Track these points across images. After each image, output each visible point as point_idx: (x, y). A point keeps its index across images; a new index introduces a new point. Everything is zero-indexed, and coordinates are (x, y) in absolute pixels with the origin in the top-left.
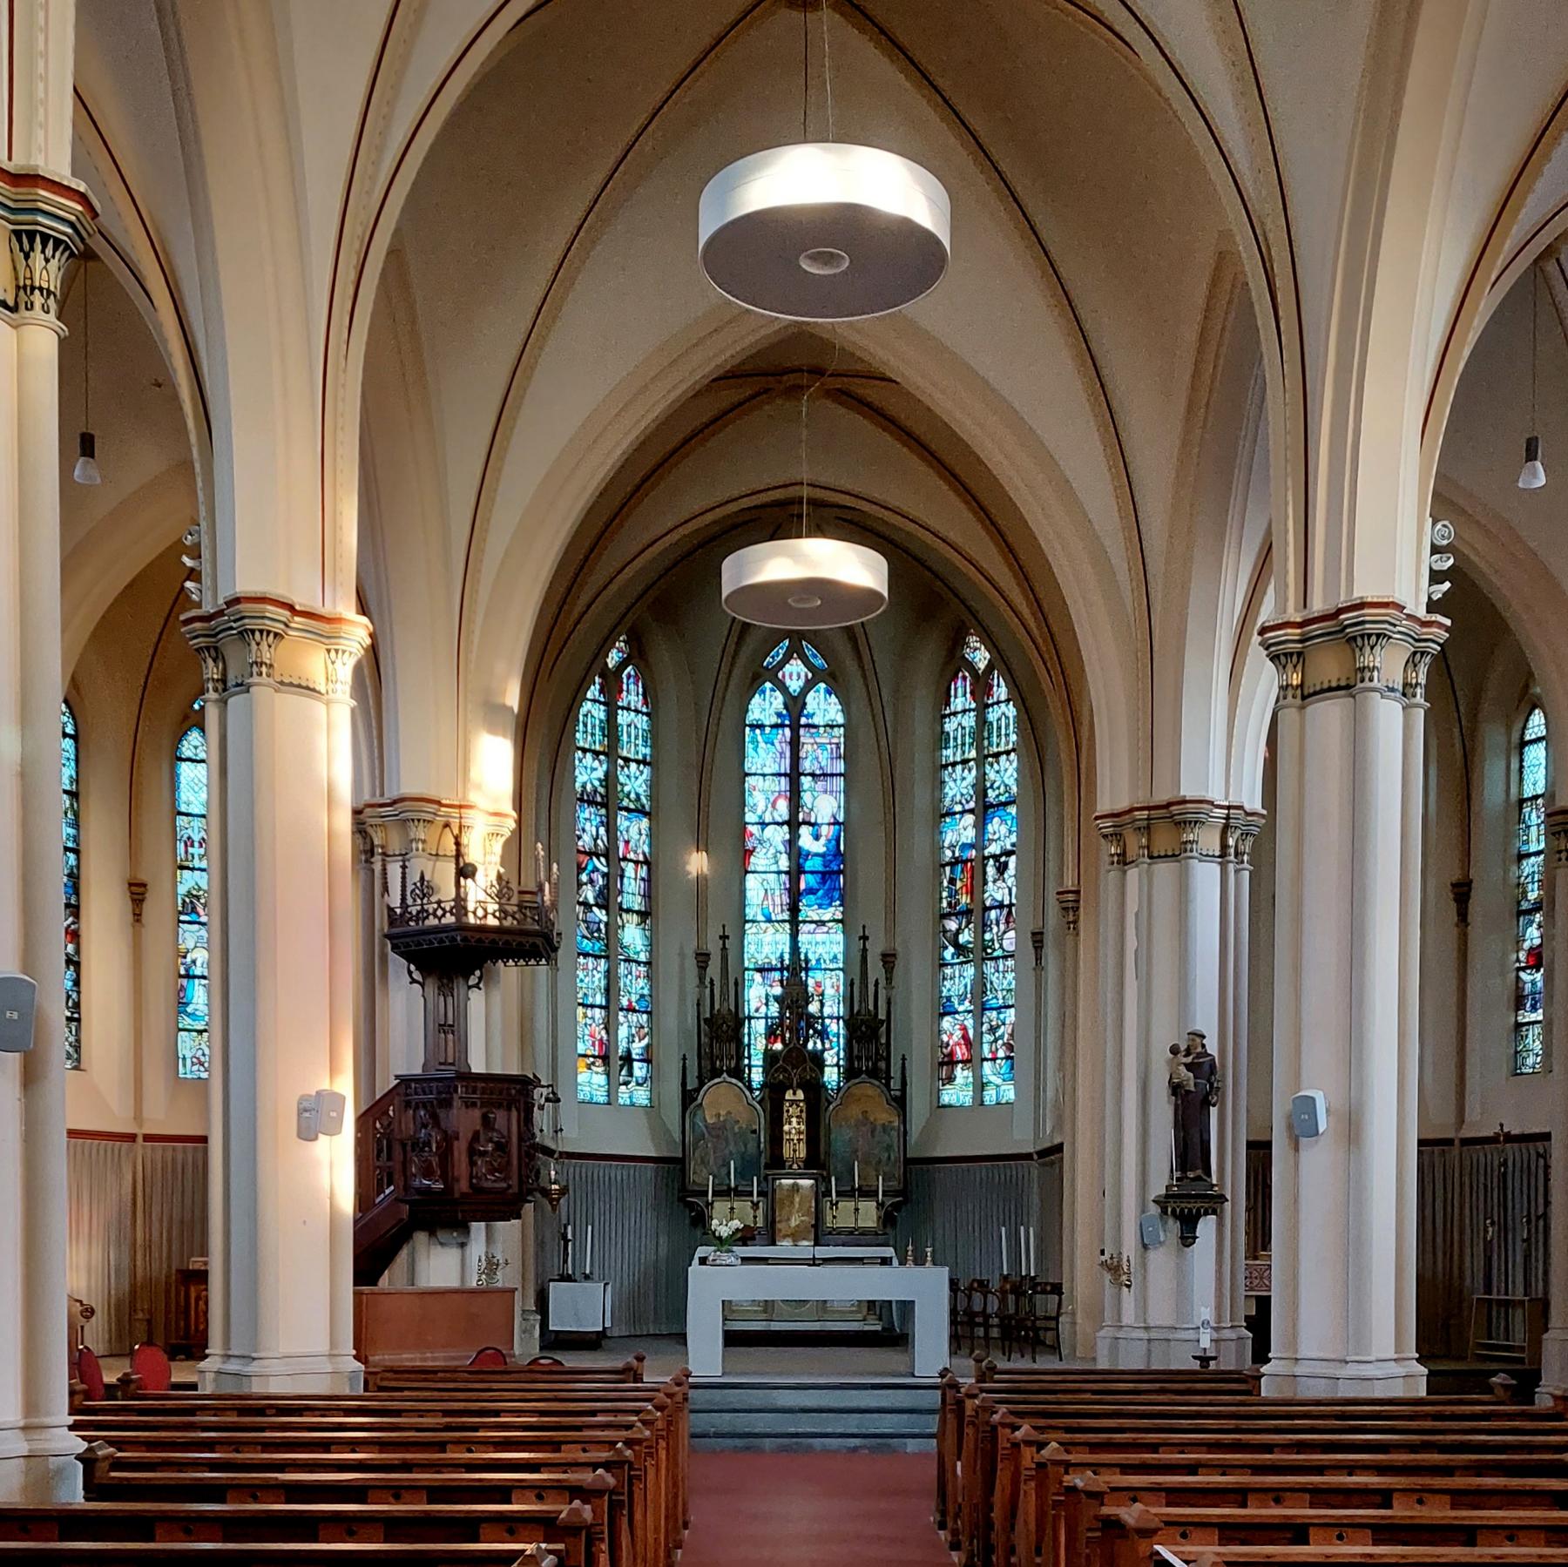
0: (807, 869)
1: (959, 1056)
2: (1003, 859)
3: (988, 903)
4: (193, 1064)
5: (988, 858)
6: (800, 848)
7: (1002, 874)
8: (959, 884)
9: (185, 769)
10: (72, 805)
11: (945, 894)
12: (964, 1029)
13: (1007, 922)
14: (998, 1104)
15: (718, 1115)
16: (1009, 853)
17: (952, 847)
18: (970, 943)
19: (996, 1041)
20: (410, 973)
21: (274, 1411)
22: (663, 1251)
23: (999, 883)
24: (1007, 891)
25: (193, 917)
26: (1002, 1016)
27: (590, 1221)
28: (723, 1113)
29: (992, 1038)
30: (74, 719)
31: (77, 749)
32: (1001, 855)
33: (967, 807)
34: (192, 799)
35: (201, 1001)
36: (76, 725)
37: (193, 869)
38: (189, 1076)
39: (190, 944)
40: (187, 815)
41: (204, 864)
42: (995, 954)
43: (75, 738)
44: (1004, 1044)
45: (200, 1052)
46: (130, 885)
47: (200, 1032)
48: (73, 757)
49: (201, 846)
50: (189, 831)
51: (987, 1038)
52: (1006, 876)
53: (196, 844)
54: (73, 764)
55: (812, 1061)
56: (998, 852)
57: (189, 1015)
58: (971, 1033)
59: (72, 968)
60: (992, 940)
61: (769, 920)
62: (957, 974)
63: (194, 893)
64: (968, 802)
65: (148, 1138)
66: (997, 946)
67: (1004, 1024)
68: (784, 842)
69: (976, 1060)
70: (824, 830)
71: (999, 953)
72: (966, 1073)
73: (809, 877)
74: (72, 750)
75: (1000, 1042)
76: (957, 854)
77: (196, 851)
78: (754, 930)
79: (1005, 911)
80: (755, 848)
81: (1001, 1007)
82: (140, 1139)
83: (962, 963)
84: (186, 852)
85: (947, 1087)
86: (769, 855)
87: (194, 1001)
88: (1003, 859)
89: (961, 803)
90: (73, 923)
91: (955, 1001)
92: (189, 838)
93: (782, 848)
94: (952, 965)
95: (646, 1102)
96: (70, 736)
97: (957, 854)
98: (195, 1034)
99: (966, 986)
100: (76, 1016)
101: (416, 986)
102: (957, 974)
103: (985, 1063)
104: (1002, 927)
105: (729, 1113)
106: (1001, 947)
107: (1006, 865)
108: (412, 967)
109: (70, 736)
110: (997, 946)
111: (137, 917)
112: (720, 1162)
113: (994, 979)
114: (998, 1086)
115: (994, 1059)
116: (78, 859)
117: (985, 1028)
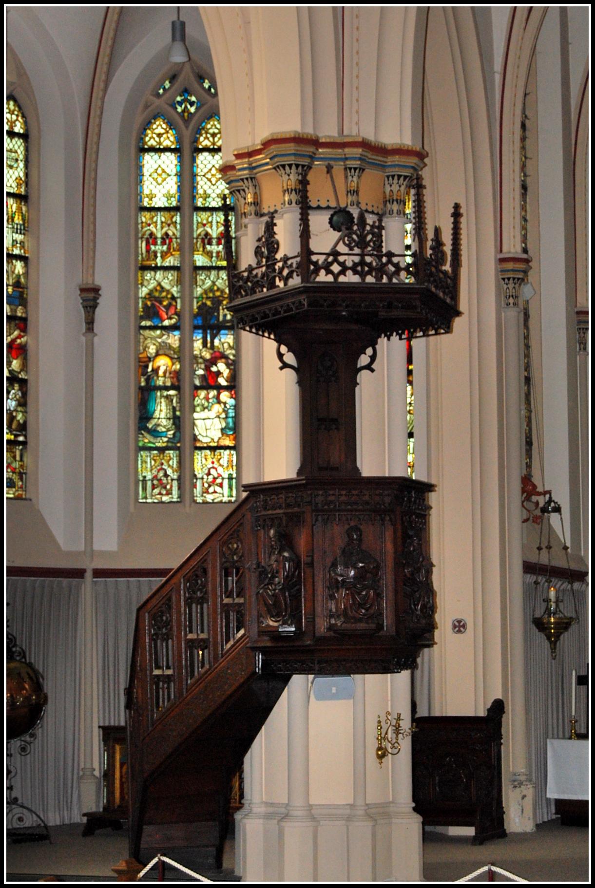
4: (154, 487)
9: (150, 161)
10: (19, 209)
14: (194, 419)
20: (280, 356)
25: (156, 322)
30: (23, 117)
31: (27, 149)
34: (209, 192)
35: (163, 415)
36: (26, 123)
37: (156, 268)
38: (149, 501)
39: (152, 350)
40: (205, 209)
41: (170, 261)
43: (25, 137)
45: (161, 474)
46: (82, 290)
47: (162, 450)
48: (21, 157)
49: (163, 243)
50: (152, 228)
53: (214, 241)
54: (22, 165)
57: (149, 431)
59: (17, 386)
63: (157, 294)
65: (99, 573)
74: (21, 151)
77: (159, 248)
82: (89, 575)
84: (148, 250)
87: (157, 414)
90: (19, 337)
92: (151, 234)
96: (19, 135)
98: (208, 452)
100: (21, 439)
101: (288, 371)
108: (284, 349)
109: (19, 135)
111: (90, 323)
116: (26, 265)
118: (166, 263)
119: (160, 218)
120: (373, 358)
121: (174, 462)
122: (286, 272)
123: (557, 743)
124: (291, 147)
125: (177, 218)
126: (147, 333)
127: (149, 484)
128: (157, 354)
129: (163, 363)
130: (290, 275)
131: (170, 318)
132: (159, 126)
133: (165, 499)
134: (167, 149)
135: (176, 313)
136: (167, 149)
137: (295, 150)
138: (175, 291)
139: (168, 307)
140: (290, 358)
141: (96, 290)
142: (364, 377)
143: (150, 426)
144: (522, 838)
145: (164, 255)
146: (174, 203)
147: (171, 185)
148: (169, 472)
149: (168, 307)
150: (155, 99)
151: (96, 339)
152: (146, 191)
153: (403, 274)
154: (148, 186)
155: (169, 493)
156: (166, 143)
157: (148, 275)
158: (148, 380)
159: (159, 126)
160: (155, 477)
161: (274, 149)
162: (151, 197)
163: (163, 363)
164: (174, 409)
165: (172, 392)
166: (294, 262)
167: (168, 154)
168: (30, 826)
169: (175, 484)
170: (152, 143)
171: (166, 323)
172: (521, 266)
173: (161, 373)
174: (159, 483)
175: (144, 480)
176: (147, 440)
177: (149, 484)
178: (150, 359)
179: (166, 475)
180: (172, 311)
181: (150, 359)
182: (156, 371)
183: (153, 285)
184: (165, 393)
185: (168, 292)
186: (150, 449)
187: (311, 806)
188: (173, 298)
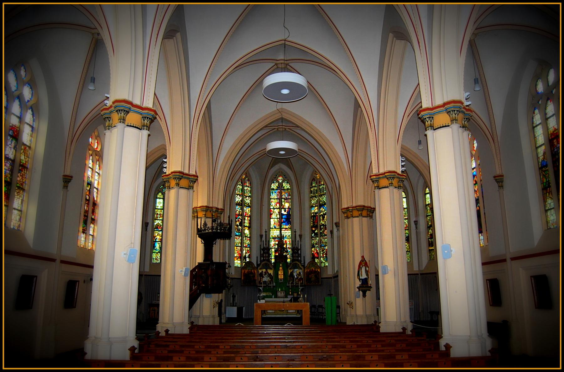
4: (155, 260)
6: (282, 213)
9: (158, 200)
19: (324, 253)
20: (202, 241)
25: (157, 229)
35: (158, 247)
37: (158, 220)
39: (156, 235)
41: (161, 218)
47: (157, 253)
49: (160, 215)
50: (158, 212)
57: (155, 249)
61: (275, 228)
65: (145, 275)
70: (287, 210)
73: (284, 219)
77: (159, 216)
78: (272, 230)
80: (272, 213)
86: (275, 215)
92: (158, 213)
93: (278, 213)
101: (202, 244)
106: (324, 234)
108: (202, 240)
114: (324, 263)
118: (160, 219)
119: (159, 210)
120: (216, 242)
121: (159, 255)
122: (208, 229)
123: (229, 307)
124: (205, 208)
125: (162, 211)
126: (156, 231)
127: (154, 259)
128: (157, 235)
129: (158, 237)
130: (209, 230)
131: (160, 229)
132: (160, 194)
133: (157, 262)
134: (161, 198)
135: (161, 228)
136: (161, 198)
137: (206, 209)
138: (161, 224)
139: (160, 227)
140: (203, 242)
141: (148, 223)
142: (214, 245)
143: (155, 248)
144: (224, 323)
145: (160, 217)
146: (162, 208)
147: (162, 205)
148: (158, 257)
149: (160, 227)
150: (160, 189)
151: (147, 232)
152: (157, 206)
153: (226, 231)
154: (157, 205)
155: (158, 261)
156: (161, 197)
157: (157, 221)
158: (155, 240)
159: (160, 194)
160: (156, 258)
161: (202, 208)
162: (158, 207)
163: (158, 237)
164: (160, 246)
165: (160, 242)
166: (210, 228)
167: (161, 199)
168: (551, 210)
169: (159, 259)
170: (159, 197)
171: (159, 230)
172: (70, 178)
173: (158, 239)
174: (156, 259)
175: (154, 258)
176: (154, 251)
177: (154, 259)
178: (156, 236)
179: (158, 258)
180: (160, 228)
181: (156, 236)
182: (157, 238)
183: (157, 222)
184: (158, 243)
185: (160, 224)
186: (155, 253)
187: (174, 323)
188: (161, 225)
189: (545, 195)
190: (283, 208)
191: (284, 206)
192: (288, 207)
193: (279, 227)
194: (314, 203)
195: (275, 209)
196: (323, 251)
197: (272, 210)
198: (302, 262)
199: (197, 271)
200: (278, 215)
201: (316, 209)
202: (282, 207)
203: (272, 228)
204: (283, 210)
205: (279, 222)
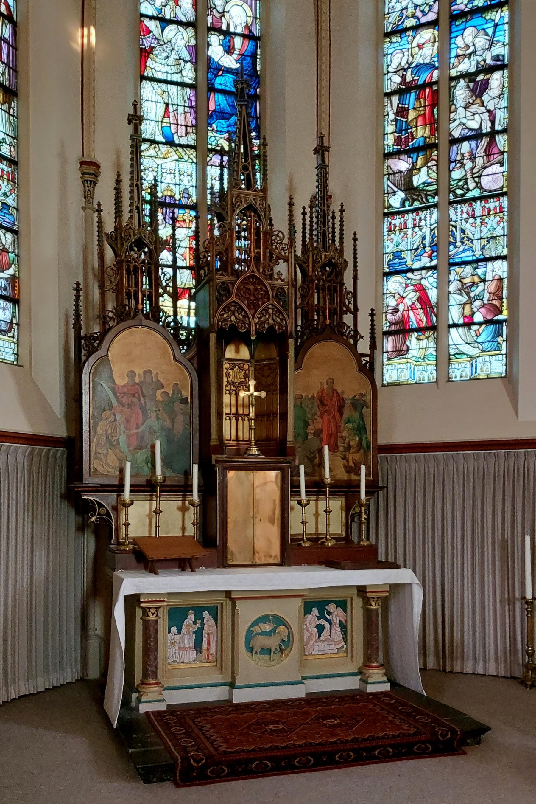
0: (217, 86)
1: (414, 324)
2: (480, 78)
3: (456, 134)
5: (457, 78)
6: (209, 58)
7: (480, 96)
8: (412, 115)
11: (390, 129)
12: (420, 289)
13: (488, 153)
15: (132, 374)
16: (490, 70)
17: (402, 70)
18: (429, 184)
19: (471, 301)
21: (120, 296)
22: (40, 572)
23: (474, 108)
24: (486, 116)
26: (480, 272)
27: (527, 529)
28: (139, 371)
29: (465, 299)
32: (478, 73)
33: (423, 20)
42: (469, 195)
44: (484, 305)
51: (456, 299)
52: (485, 97)
55: (276, 297)
56: (473, 70)
58: (433, 295)
60: (465, 179)
61: (170, 143)
62: (410, 224)
64: (424, 14)
66: (472, 185)
67: (484, 281)
68: (188, 47)
69: (442, 327)
70: (238, 42)
71: (476, 193)
72: (424, 343)
73: (220, 98)
75: (478, 303)
76: (409, 79)
78: (152, 152)
79: (485, 141)
80: (152, 48)
81: (478, 261)
83: (417, 210)
85: (397, 360)
86: (171, 61)
88: (480, 78)
89: (414, 16)
91: (408, 257)
93: (185, 54)
94: (401, 213)
95: (12, 358)
97: (409, 79)
99: (424, 238)
102: (410, 224)
103: (453, 331)
104: (480, 162)
105: (148, 372)
106: (478, 185)
107: (485, 86)
110: (472, 185)
112: (135, 442)
113: (467, 227)
114: (471, 358)
115: (469, 323)
117: (453, 287)
189: (403, 128)
190: (216, 29)
191: (222, 14)
192: (247, 27)
193: (191, 140)
194: (411, 10)
195: (171, 22)
196: (465, 289)
197: (152, 25)
198: (360, 342)
199: (193, 333)
200: (189, 65)
201: (420, 47)
202: (209, 19)
203: (153, 142)
204: (215, 39)
205: (196, 109)
